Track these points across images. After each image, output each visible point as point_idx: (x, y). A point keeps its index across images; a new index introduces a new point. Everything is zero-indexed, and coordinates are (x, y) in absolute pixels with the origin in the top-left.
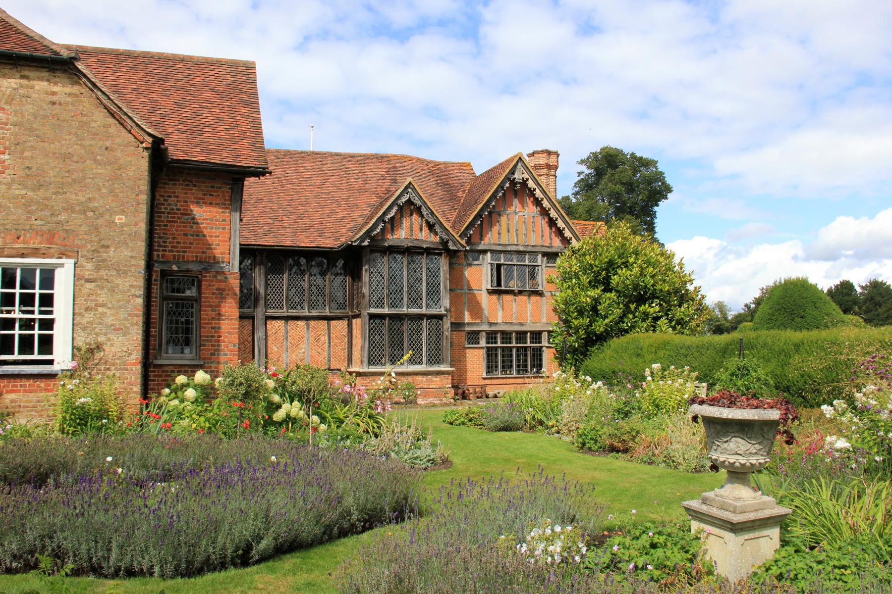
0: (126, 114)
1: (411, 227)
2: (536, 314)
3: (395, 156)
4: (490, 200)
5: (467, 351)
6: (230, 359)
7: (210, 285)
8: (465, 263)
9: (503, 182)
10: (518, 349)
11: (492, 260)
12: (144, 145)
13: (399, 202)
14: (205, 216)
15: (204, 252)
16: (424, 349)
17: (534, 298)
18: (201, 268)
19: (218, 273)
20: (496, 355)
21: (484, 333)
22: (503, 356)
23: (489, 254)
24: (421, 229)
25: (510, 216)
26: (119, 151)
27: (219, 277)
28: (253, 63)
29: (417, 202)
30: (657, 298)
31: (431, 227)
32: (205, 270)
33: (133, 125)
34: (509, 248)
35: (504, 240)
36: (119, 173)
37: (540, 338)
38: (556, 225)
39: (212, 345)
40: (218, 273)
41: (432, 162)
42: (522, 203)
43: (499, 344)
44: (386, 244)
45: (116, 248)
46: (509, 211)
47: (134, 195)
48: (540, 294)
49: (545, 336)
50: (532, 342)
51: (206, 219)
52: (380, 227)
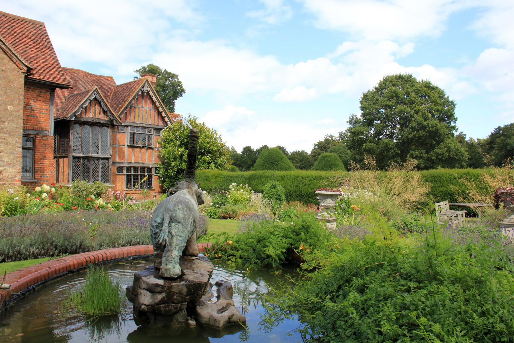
0: (14, 54)
1: (95, 112)
2: (148, 158)
3: (74, 69)
4: (131, 100)
5: (117, 176)
6: (49, 179)
7: (40, 142)
8: (117, 131)
9: (138, 92)
10: (134, 175)
11: (130, 130)
12: (22, 71)
13: (90, 98)
14: (37, 106)
15: (37, 125)
16: (100, 175)
17: (149, 151)
18: (36, 133)
19: (44, 136)
20: (131, 179)
21: (125, 168)
22: (134, 179)
23: (129, 128)
24: (100, 113)
25: (140, 109)
26: (9, 73)
27: (44, 138)
28: (43, 23)
29: (100, 100)
30: (210, 153)
31: (105, 112)
32: (37, 134)
33: (17, 60)
34: (139, 125)
35: (137, 121)
36: (9, 84)
37: (151, 171)
38: (161, 115)
39: (41, 172)
40: (44, 136)
41: (93, 75)
42: (146, 102)
43: (132, 173)
44: (82, 120)
45: (9, 123)
46: (140, 106)
47: (17, 96)
48: (151, 148)
49: (153, 170)
50: (134, 172)
51: (37, 108)
52: (80, 111)
